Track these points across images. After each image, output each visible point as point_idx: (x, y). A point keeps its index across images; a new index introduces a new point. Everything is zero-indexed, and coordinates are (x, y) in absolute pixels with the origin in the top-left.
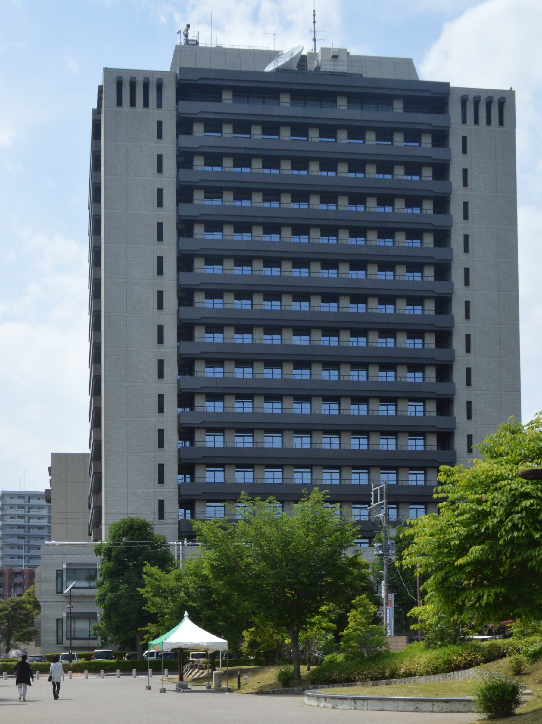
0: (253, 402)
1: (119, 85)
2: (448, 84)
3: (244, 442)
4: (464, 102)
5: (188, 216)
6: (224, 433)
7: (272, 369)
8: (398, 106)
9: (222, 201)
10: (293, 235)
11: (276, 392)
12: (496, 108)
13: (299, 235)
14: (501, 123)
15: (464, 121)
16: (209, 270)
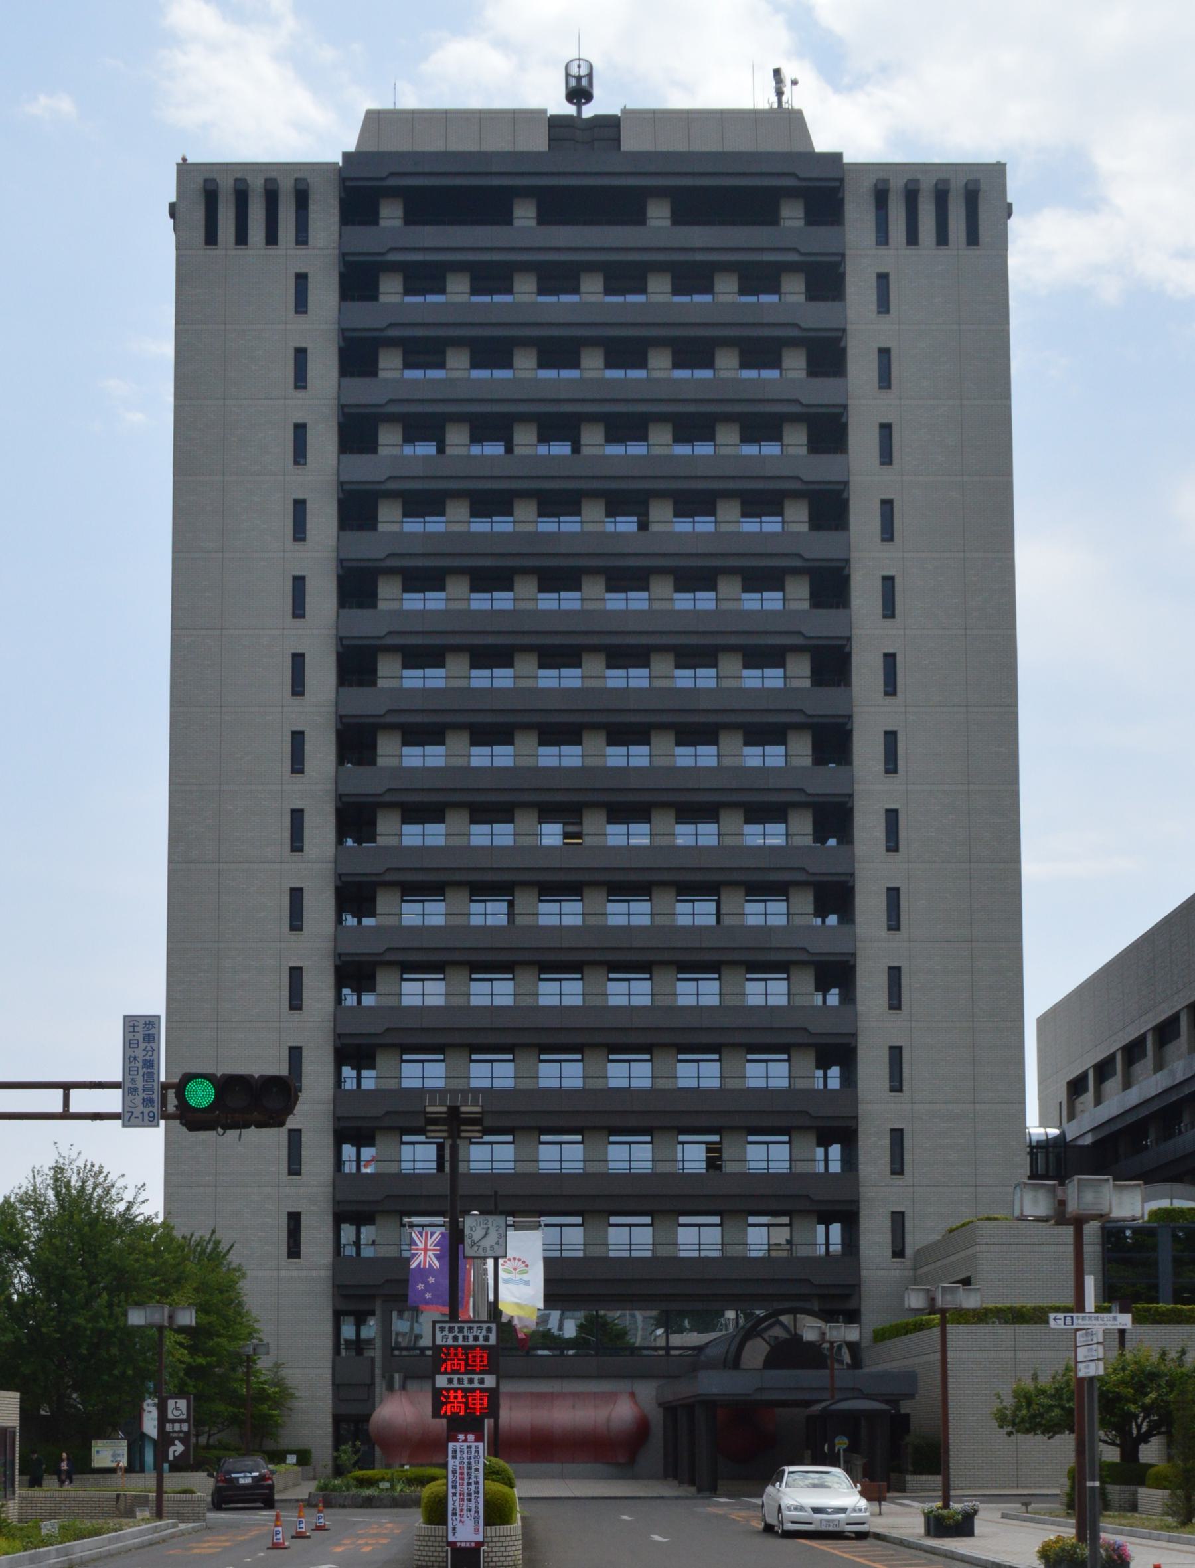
0: (787, 900)
1: (211, 197)
2: (839, 156)
3: (629, 993)
4: (881, 197)
5: (830, 483)
6: (787, 972)
7: (695, 823)
8: (659, 214)
9: (782, 445)
10: (676, 516)
11: (773, 877)
12: (958, 207)
13: (692, 516)
14: (973, 239)
15: (883, 238)
16: (413, 602)
